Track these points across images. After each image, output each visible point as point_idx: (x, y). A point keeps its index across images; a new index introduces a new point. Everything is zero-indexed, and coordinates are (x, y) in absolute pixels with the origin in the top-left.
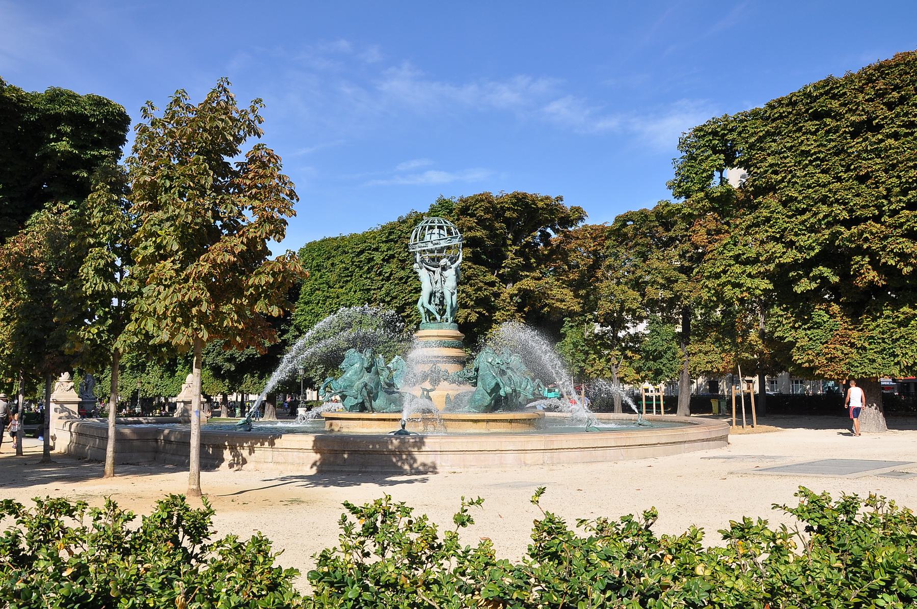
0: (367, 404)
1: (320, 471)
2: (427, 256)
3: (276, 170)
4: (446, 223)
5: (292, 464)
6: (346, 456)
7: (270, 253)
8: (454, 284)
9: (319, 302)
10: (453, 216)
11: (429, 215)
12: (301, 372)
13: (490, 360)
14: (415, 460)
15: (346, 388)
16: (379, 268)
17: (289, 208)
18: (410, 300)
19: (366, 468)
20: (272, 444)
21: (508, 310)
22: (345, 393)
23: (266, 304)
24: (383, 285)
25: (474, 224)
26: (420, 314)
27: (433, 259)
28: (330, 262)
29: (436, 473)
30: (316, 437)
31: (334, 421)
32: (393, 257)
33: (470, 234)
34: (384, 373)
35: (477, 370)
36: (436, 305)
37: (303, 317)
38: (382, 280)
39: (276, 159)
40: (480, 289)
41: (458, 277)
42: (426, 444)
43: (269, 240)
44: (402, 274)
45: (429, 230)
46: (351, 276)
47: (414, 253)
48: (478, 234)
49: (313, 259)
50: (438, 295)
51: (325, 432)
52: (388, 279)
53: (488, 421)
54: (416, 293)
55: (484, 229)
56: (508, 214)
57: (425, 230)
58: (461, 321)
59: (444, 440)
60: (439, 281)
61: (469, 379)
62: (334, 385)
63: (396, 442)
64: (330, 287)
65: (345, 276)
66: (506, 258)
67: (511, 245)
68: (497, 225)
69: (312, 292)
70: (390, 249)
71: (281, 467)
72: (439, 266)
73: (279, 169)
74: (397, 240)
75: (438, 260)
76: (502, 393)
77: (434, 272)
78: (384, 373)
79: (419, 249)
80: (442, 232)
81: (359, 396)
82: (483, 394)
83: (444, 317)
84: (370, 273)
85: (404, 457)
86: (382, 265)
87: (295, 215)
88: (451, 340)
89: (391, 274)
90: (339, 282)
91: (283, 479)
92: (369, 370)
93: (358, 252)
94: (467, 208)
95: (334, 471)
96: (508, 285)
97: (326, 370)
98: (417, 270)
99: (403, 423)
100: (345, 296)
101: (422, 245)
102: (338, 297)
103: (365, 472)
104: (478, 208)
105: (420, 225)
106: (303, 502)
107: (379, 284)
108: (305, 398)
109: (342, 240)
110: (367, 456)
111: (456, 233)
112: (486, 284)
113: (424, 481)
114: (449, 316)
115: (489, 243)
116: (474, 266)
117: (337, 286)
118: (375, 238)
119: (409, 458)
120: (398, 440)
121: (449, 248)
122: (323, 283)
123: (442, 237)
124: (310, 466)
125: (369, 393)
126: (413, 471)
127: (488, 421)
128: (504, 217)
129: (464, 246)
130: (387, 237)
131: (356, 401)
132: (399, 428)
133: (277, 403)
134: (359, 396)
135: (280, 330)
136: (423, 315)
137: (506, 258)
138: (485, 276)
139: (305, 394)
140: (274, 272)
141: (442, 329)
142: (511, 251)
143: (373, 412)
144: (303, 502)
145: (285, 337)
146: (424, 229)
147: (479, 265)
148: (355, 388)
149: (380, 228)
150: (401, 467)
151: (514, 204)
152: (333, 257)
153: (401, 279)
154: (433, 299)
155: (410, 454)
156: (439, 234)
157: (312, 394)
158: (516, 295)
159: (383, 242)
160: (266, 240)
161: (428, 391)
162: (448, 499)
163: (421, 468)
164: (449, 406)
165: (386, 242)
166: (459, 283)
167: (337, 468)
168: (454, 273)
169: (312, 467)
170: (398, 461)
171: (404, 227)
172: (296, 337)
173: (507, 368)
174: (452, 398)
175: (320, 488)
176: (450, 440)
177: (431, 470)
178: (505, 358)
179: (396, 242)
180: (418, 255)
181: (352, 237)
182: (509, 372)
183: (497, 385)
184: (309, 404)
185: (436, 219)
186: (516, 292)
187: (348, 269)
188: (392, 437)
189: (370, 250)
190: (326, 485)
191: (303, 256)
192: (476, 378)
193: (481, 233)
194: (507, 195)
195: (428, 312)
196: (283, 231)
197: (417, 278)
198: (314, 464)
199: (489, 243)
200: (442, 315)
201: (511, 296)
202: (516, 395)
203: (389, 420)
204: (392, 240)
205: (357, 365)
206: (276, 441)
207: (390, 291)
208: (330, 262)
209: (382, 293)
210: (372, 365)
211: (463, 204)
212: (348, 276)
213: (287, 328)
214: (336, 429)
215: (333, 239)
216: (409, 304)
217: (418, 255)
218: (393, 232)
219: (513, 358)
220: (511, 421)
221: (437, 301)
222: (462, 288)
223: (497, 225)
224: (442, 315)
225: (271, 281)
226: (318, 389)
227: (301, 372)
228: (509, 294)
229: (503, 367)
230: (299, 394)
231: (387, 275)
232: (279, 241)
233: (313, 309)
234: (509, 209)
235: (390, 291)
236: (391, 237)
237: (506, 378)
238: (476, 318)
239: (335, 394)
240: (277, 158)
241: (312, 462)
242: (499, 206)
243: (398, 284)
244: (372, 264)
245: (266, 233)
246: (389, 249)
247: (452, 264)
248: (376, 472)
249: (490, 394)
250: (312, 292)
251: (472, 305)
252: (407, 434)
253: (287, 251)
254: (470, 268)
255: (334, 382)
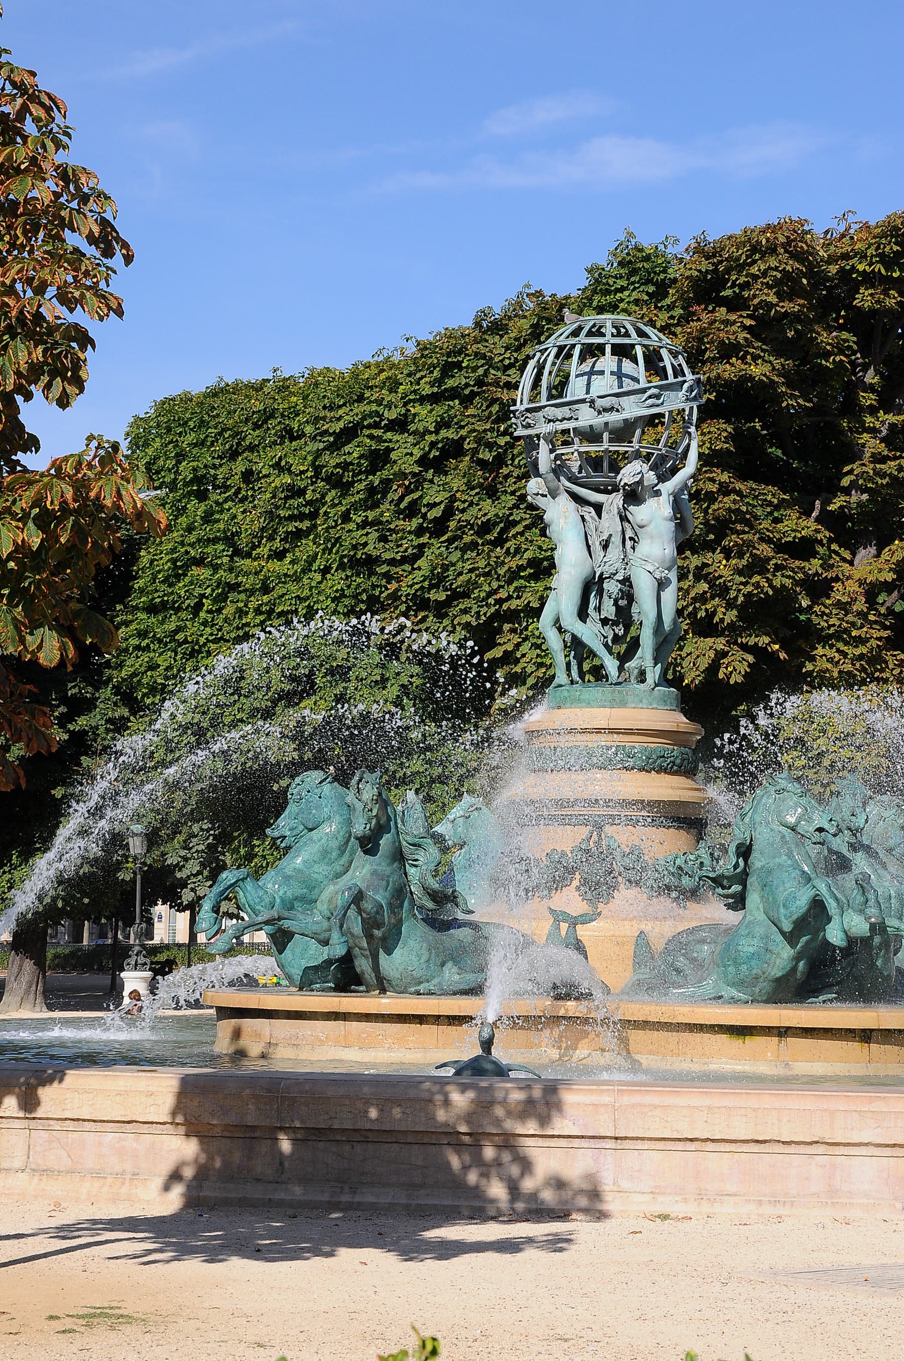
0: (363, 965)
1: (192, 1202)
2: (573, 454)
3: (50, 146)
4: (641, 334)
5: (98, 1175)
6: (286, 1145)
7: (32, 444)
8: (669, 550)
9: (199, 606)
10: (670, 308)
11: (584, 304)
12: (136, 846)
13: (791, 820)
14: (526, 1165)
15: (289, 905)
16: (408, 491)
17: (94, 288)
18: (514, 604)
19: (353, 1190)
20: (29, 1103)
21: (861, 641)
22: (286, 924)
23: (16, 623)
24: (422, 547)
25: (743, 335)
26: (547, 652)
27: (595, 463)
28: (240, 466)
29: (601, 1216)
30: (185, 1082)
31: (247, 1023)
32: (454, 449)
33: (728, 370)
34: (421, 856)
35: (745, 851)
36: (605, 622)
37: (145, 657)
38: (420, 532)
39: (48, 110)
40: (758, 566)
41: (681, 524)
42: (568, 1109)
43: (28, 396)
44: (489, 509)
45: (582, 359)
46: (313, 516)
47: (531, 443)
48: (757, 370)
49: (180, 457)
50: (612, 587)
51: (213, 1059)
52: (439, 527)
53: (783, 1032)
54: (535, 577)
55: (778, 354)
56: (865, 299)
57: (569, 356)
58: (693, 677)
59: (626, 1100)
60: (616, 540)
61: (717, 881)
62: (248, 893)
63: (460, 1100)
64: (237, 552)
65: (291, 518)
66: (853, 454)
67: (873, 411)
68: (825, 338)
69: (178, 572)
70: (447, 426)
71: (55, 1188)
72: (615, 489)
73: (58, 145)
74: (473, 394)
75: (615, 468)
76: (834, 935)
77: (598, 508)
78: (421, 856)
79: (545, 429)
80: (627, 366)
81: (335, 937)
82: (766, 937)
83: (631, 665)
84: (376, 505)
85: (489, 1153)
86: (419, 481)
87: (120, 313)
88: (654, 744)
89: (449, 512)
90: (271, 538)
91: (64, 1231)
92: (369, 845)
93: (338, 436)
94: (719, 281)
95: (245, 1204)
96: (862, 553)
97: (224, 839)
98: (541, 502)
99: (486, 1034)
100: (292, 587)
101: (559, 413)
102: (266, 589)
103: (358, 1206)
104: (755, 277)
105: (552, 344)
106: (128, 1319)
107: (408, 545)
108: (150, 934)
109: (280, 390)
110: (358, 1148)
111: (678, 372)
112: (781, 548)
113: (557, 1244)
114: (648, 662)
115: (793, 402)
116: (739, 486)
117: (264, 550)
118: (392, 386)
119: (506, 1157)
120: (471, 1095)
121: (653, 421)
122: (215, 541)
123: (628, 385)
124: (159, 1182)
125: (370, 924)
126: (520, 1206)
127: (783, 1032)
128: (850, 307)
129: (707, 413)
130: (440, 381)
131: (325, 953)
132: (470, 1051)
133: (50, 953)
134: (335, 937)
135: (64, 700)
136: (560, 659)
137: (853, 454)
138: (777, 521)
139: (150, 922)
140: (45, 512)
141: (623, 704)
142: (874, 431)
143: (383, 991)
144: (128, 1319)
145: (82, 722)
146: (564, 353)
147: (759, 481)
148: (322, 906)
149: (411, 349)
150: (477, 1193)
151: (888, 261)
152: (252, 448)
153: (485, 528)
154: (593, 602)
155: (508, 1142)
156: (619, 375)
157: (172, 921)
158: (888, 587)
159: (422, 400)
160: (19, 399)
161: (574, 922)
162: (642, 1318)
163: (548, 1196)
164: (645, 973)
165: (434, 399)
166: (684, 546)
167: (255, 1192)
168: (668, 511)
169: (167, 1188)
170: (465, 1168)
171: (496, 345)
172: (119, 726)
173: (853, 847)
174: (658, 945)
175: (194, 1266)
176: (648, 1099)
177: (583, 1202)
178: (846, 813)
179: (467, 401)
180: (544, 447)
181: (314, 381)
182: (860, 862)
183: (818, 907)
184: (162, 957)
185: (607, 319)
186: (890, 577)
187: (302, 492)
188: (442, 1082)
189: (376, 426)
190: (213, 1255)
191: (146, 444)
192: (743, 878)
193: (766, 369)
194: (866, 227)
195: (576, 646)
196: (77, 364)
197: (538, 522)
198: (175, 1176)
199: (793, 402)
200: (623, 659)
201: (872, 591)
202: (886, 944)
203: (437, 1019)
204: (454, 393)
205: (328, 829)
206: (45, 1093)
207: (445, 568)
208: (240, 466)
209: (418, 575)
210: (381, 829)
211: (705, 266)
212: (301, 517)
213: (88, 692)
214: (254, 1050)
215: (251, 386)
216: (512, 616)
217: (544, 447)
218: (458, 365)
219: (873, 809)
220: (865, 1036)
221: (609, 610)
222: (695, 561)
223: (825, 338)
224: (623, 659)
225: (36, 541)
226: (193, 907)
227: (136, 846)
228: (861, 582)
229: (840, 844)
230: (129, 922)
231: (436, 513)
232: (63, 402)
233: (179, 630)
234: (869, 279)
235: (445, 568)
236: (450, 383)
237: (848, 880)
238: (744, 668)
239: (256, 926)
240: (51, 105)
241: (165, 1168)
242: (833, 269)
243: (473, 546)
244: (385, 474)
245: (18, 374)
246: (442, 424)
247: (662, 478)
248: (389, 1210)
249: (791, 938)
250: (178, 572)
251: (732, 625)
252: (501, 1072)
253: (90, 438)
254: (725, 490)
255: (249, 885)
